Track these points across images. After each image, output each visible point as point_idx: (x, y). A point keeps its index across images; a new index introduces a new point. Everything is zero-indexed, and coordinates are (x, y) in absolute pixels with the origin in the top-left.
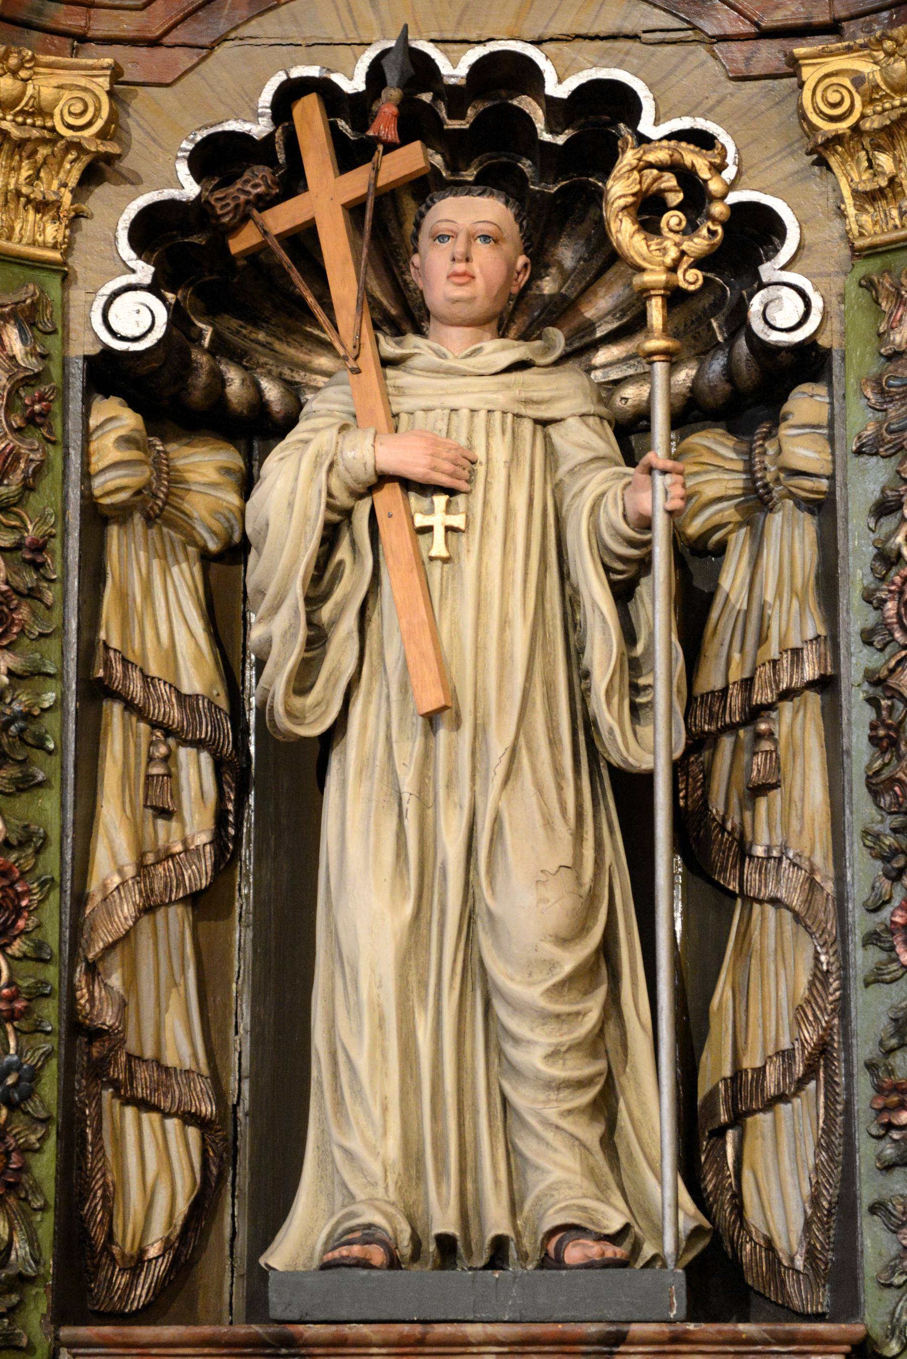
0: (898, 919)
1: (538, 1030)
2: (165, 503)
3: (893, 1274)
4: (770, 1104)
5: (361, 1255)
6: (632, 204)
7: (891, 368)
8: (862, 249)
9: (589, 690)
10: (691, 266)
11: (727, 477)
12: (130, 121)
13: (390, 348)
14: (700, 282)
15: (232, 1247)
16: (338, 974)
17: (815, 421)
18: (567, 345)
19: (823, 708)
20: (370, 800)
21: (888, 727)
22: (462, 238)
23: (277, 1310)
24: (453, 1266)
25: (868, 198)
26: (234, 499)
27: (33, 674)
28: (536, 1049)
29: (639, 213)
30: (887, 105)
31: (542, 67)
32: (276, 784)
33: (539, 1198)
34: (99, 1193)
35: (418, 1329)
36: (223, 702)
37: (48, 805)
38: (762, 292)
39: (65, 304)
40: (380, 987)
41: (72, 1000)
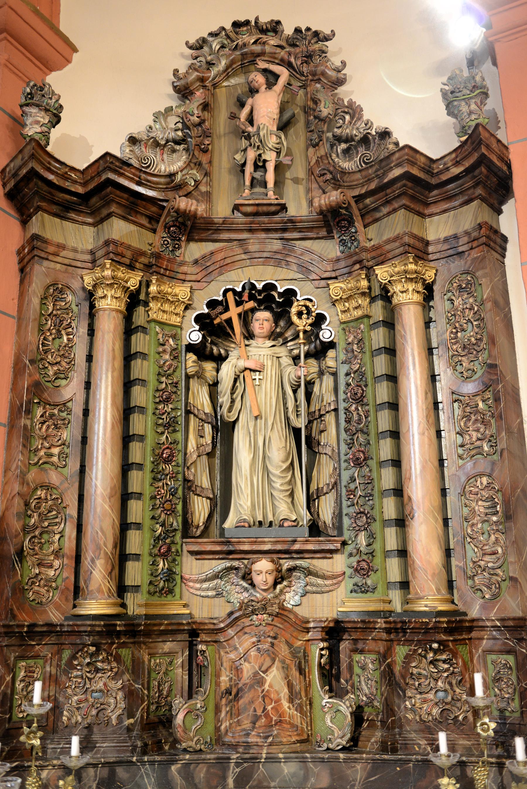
4: (324, 494)
13: (247, 342)
23: (226, 536)
25: (344, 312)
26: (215, 373)
28: (278, 484)
32: (225, 431)
36: (213, 414)
39: (181, 334)
41: (184, 474)
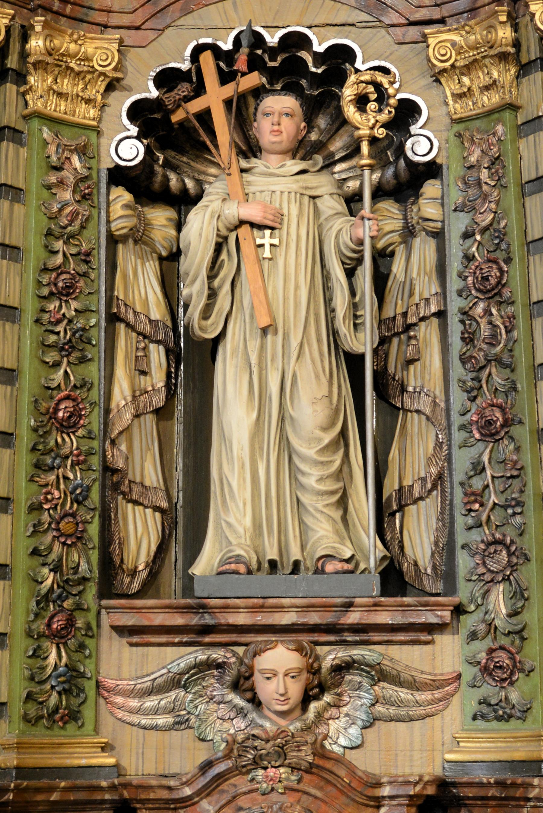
0: (474, 419)
1: (313, 469)
2: (143, 234)
3: (472, 576)
5: (235, 569)
6: (354, 99)
7: (470, 172)
8: (456, 120)
9: (335, 317)
10: (381, 127)
11: (395, 222)
12: (127, 63)
13: (244, 164)
14: (385, 134)
15: (175, 566)
16: (223, 445)
17: (435, 197)
18: (324, 162)
19: (439, 325)
20: (237, 367)
21: (469, 333)
22: (276, 115)
24: (276, 573)
26: (173, 232)
27: (86, 311)
28: (312, 477)
29: (358, 102)
30: (467, 55)
31: (311, 38)
32: (194, 360)
33: (314, 543)
34: (117, 541)
35: (261, 601)
36: (169, 323)
37: (93, 369)
38: (412, 139)
39: (98, 146)
40: (242, 450)
41: (104, 456)
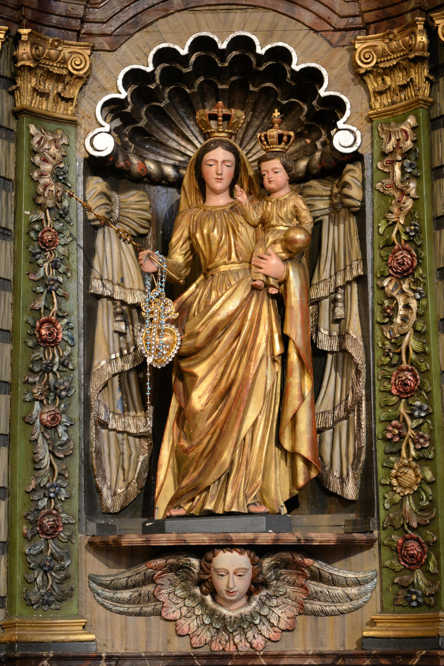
30: (389, 58)
